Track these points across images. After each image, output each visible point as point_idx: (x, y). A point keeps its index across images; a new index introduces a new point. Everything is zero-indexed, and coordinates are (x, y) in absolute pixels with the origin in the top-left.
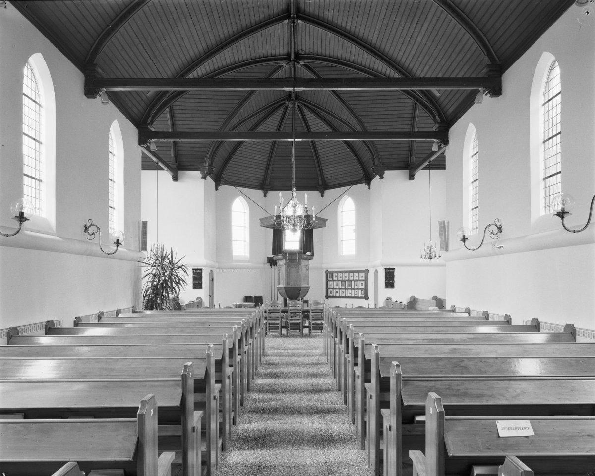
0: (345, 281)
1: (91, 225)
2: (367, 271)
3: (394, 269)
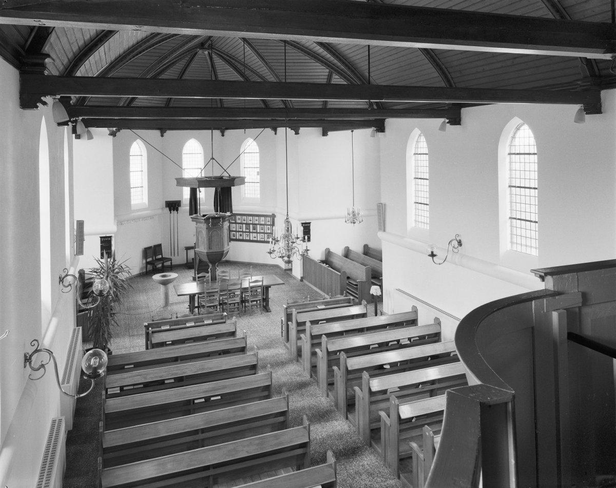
0: (249, 224)
1: (67, 275)
2: (273, 216)
3: (310, 223)
